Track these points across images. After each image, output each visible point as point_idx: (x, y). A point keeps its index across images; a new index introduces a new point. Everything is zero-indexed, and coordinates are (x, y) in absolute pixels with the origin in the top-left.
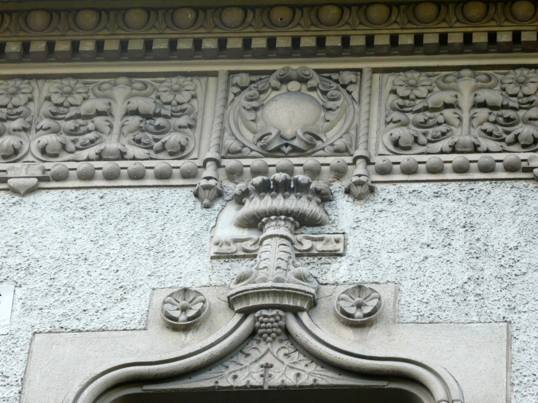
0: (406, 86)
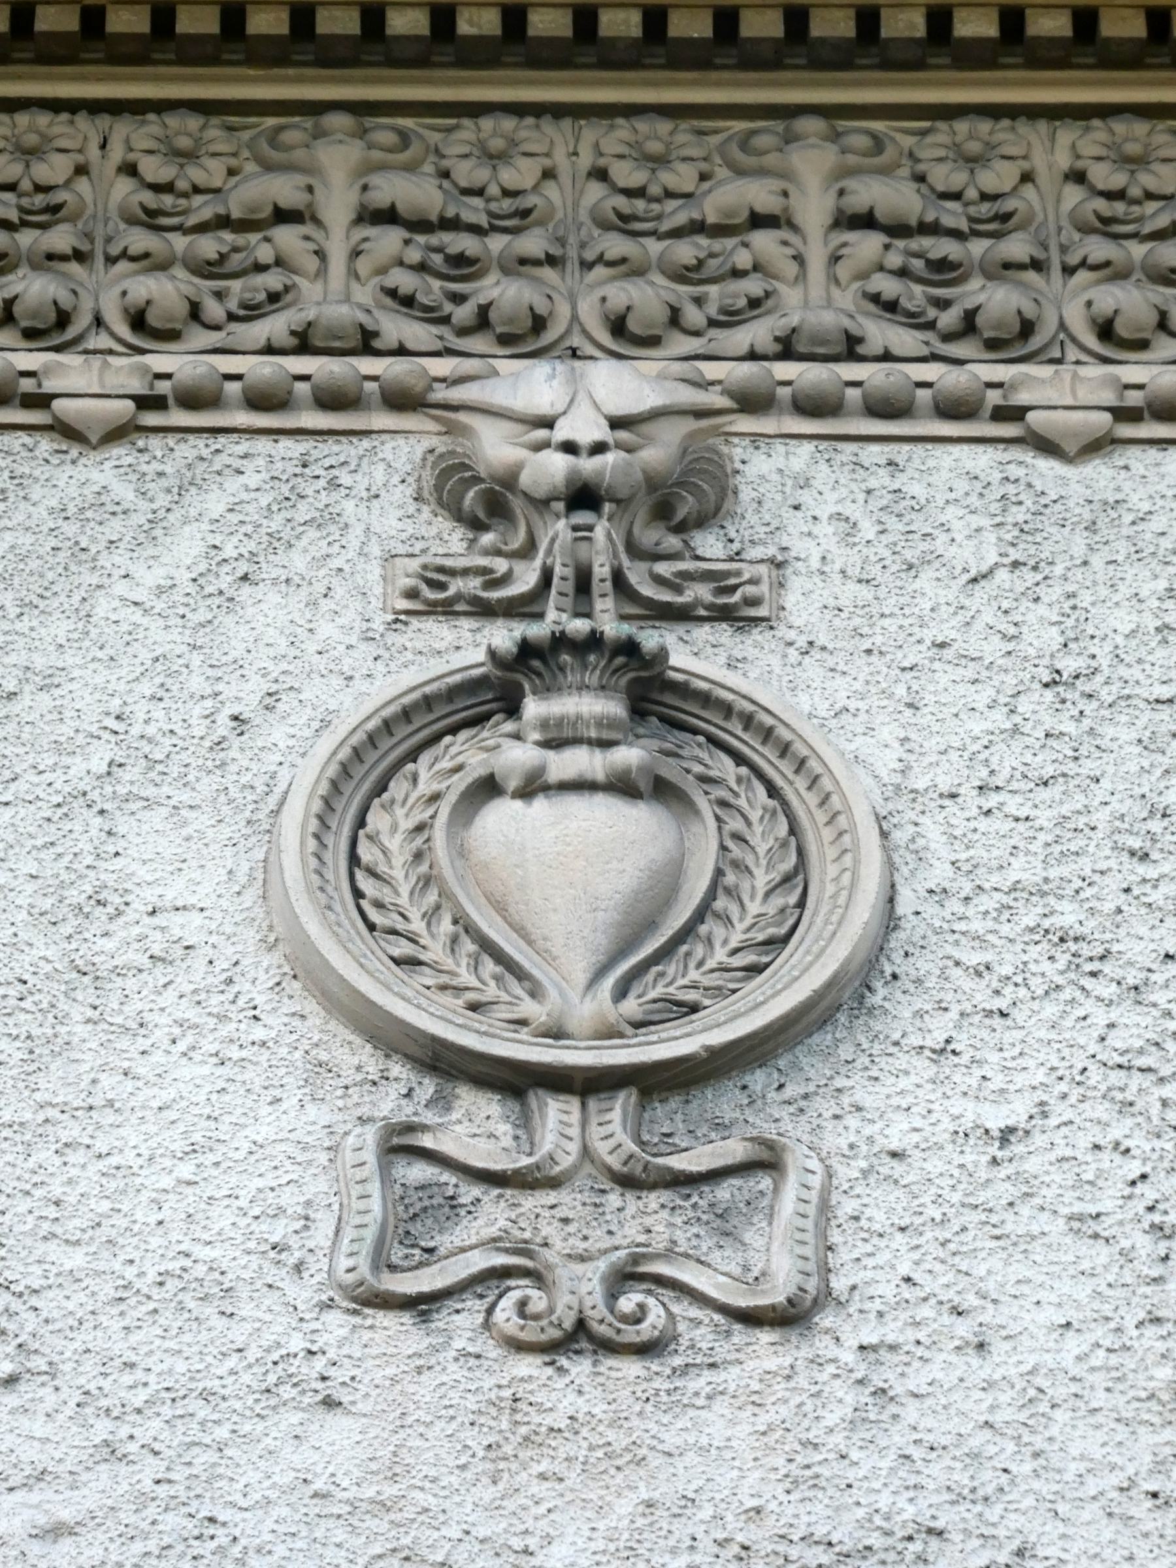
0: (955, 161)
